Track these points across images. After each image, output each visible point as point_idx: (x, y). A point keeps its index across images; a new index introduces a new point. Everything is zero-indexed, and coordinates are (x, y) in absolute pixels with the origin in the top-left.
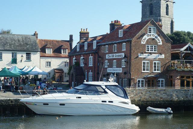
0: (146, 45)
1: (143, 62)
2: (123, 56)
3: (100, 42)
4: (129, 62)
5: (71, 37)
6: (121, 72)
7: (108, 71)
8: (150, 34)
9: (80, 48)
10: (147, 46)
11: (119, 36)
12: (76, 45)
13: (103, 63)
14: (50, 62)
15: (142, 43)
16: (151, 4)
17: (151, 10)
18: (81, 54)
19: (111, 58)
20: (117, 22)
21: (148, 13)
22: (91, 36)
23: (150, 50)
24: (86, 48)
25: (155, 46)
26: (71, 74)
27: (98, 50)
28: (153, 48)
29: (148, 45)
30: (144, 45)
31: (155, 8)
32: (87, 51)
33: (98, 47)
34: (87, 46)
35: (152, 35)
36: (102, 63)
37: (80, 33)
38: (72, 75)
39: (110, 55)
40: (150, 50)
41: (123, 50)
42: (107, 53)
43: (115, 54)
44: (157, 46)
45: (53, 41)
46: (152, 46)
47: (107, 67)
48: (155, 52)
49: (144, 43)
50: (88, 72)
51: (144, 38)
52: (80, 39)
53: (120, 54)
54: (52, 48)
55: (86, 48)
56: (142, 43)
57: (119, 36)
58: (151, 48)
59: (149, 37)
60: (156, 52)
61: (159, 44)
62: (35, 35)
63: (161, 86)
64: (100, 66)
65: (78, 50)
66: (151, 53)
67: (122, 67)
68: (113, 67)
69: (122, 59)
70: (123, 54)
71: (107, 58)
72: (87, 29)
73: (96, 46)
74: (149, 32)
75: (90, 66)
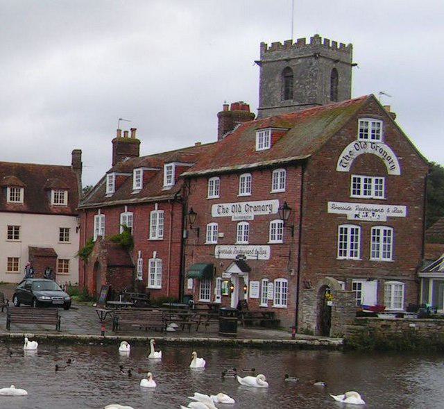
0: (353, 176)
1: (340, 227)
2: (275, 211)
3: (188, 167)
4: (297, 226)
5: (77, 154)
8: (364, 140)
9: (118, 186)
10: (355, 179)
11: (257, 149)
12: (104, 178)
13: (200, 232)
14: (17, 228)
15: (340, 169)
16: (288, 69)
17: (286, 86)
18: (152, 203)
21: (278, 95)
22: (145, 150)
23: (362, 192)
24: (137, 186)
25: (379, 178)
26: (93, 261)
27: (184, 190)
28: (373, 184)
29: (357, 177)
30: (346, 176)
31: (300, 79)
32: (141, 194)
33: (187, 182)
34: (141, 179)
35: (369, 145)
36: (198, 229)
37: (114, 142)
38: (97, 264)
39: (226, 206)
40: (362, 192)
41: (240, 195)
42: (214, 201)
44: (383, 178)
46: (368, 177)
47: (215, 242)
48: (367, 197)
49: (347, 170)
50: (146, 257)
51: (346, 152)
52: (219, 138)
54: (22, 187)
55: (137, 186)
56: (340, 169)
57: (257, 149)
58: (359, 186)
59: (361, 151)
60: (382, 198)
61: (390, 172)
63: (281, 284)
64: (192, 240)
65: (110, 191)
67: (271, 242)
68: (238, 242)
69: (270, 217)
70: (275, 205)
71: (215, 214)
72: (133, 130)
74: (361, 137)
75: (152, 238)
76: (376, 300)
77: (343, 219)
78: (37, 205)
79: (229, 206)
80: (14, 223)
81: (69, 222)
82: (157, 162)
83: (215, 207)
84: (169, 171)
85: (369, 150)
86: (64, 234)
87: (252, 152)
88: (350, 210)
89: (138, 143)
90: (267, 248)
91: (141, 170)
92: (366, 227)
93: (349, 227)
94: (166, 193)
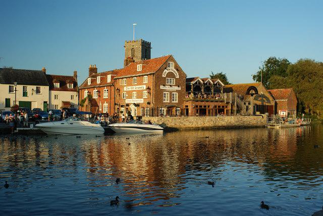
2: (145, 88)
5: (75, 73)
6: (142, 102)
7: (126, 102)
14: (24, 96)
19: (130, 90)
20: (272, 62)
32: (91, 85)
36: (118, 181)
39: (129, 87)
42: (125, 86)
43: (134, 87)
45: (59, 76)
49: (165, 76)
50: (103, 103)
51: (164, 72)
53: (140, 86)
62: (45, 70)
66: (171, 86)
70: (145, 87)
73: (110, 80)
75: (104, 97)
76: (15, 68)
77: (165, 91)
78: (63, 88)
79: (130, 87)
80: (56, 94)
81: (75, 94)
82: (104, 75)
83: (125, 88)
84: (109, 77)
85: (171, 71)
86: (72, 97)
87: (136, 72)
88: (167, 88)
89: (97, 69)
90: (142, 99)
91: (99, 77)
92: (171, 92)
93: (166, 93)
94: (108, 84)
